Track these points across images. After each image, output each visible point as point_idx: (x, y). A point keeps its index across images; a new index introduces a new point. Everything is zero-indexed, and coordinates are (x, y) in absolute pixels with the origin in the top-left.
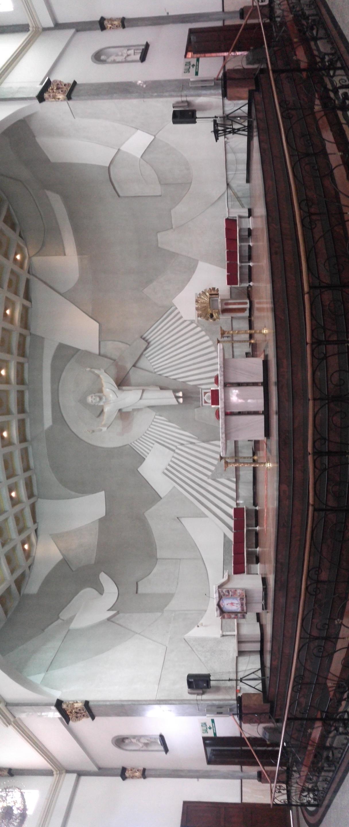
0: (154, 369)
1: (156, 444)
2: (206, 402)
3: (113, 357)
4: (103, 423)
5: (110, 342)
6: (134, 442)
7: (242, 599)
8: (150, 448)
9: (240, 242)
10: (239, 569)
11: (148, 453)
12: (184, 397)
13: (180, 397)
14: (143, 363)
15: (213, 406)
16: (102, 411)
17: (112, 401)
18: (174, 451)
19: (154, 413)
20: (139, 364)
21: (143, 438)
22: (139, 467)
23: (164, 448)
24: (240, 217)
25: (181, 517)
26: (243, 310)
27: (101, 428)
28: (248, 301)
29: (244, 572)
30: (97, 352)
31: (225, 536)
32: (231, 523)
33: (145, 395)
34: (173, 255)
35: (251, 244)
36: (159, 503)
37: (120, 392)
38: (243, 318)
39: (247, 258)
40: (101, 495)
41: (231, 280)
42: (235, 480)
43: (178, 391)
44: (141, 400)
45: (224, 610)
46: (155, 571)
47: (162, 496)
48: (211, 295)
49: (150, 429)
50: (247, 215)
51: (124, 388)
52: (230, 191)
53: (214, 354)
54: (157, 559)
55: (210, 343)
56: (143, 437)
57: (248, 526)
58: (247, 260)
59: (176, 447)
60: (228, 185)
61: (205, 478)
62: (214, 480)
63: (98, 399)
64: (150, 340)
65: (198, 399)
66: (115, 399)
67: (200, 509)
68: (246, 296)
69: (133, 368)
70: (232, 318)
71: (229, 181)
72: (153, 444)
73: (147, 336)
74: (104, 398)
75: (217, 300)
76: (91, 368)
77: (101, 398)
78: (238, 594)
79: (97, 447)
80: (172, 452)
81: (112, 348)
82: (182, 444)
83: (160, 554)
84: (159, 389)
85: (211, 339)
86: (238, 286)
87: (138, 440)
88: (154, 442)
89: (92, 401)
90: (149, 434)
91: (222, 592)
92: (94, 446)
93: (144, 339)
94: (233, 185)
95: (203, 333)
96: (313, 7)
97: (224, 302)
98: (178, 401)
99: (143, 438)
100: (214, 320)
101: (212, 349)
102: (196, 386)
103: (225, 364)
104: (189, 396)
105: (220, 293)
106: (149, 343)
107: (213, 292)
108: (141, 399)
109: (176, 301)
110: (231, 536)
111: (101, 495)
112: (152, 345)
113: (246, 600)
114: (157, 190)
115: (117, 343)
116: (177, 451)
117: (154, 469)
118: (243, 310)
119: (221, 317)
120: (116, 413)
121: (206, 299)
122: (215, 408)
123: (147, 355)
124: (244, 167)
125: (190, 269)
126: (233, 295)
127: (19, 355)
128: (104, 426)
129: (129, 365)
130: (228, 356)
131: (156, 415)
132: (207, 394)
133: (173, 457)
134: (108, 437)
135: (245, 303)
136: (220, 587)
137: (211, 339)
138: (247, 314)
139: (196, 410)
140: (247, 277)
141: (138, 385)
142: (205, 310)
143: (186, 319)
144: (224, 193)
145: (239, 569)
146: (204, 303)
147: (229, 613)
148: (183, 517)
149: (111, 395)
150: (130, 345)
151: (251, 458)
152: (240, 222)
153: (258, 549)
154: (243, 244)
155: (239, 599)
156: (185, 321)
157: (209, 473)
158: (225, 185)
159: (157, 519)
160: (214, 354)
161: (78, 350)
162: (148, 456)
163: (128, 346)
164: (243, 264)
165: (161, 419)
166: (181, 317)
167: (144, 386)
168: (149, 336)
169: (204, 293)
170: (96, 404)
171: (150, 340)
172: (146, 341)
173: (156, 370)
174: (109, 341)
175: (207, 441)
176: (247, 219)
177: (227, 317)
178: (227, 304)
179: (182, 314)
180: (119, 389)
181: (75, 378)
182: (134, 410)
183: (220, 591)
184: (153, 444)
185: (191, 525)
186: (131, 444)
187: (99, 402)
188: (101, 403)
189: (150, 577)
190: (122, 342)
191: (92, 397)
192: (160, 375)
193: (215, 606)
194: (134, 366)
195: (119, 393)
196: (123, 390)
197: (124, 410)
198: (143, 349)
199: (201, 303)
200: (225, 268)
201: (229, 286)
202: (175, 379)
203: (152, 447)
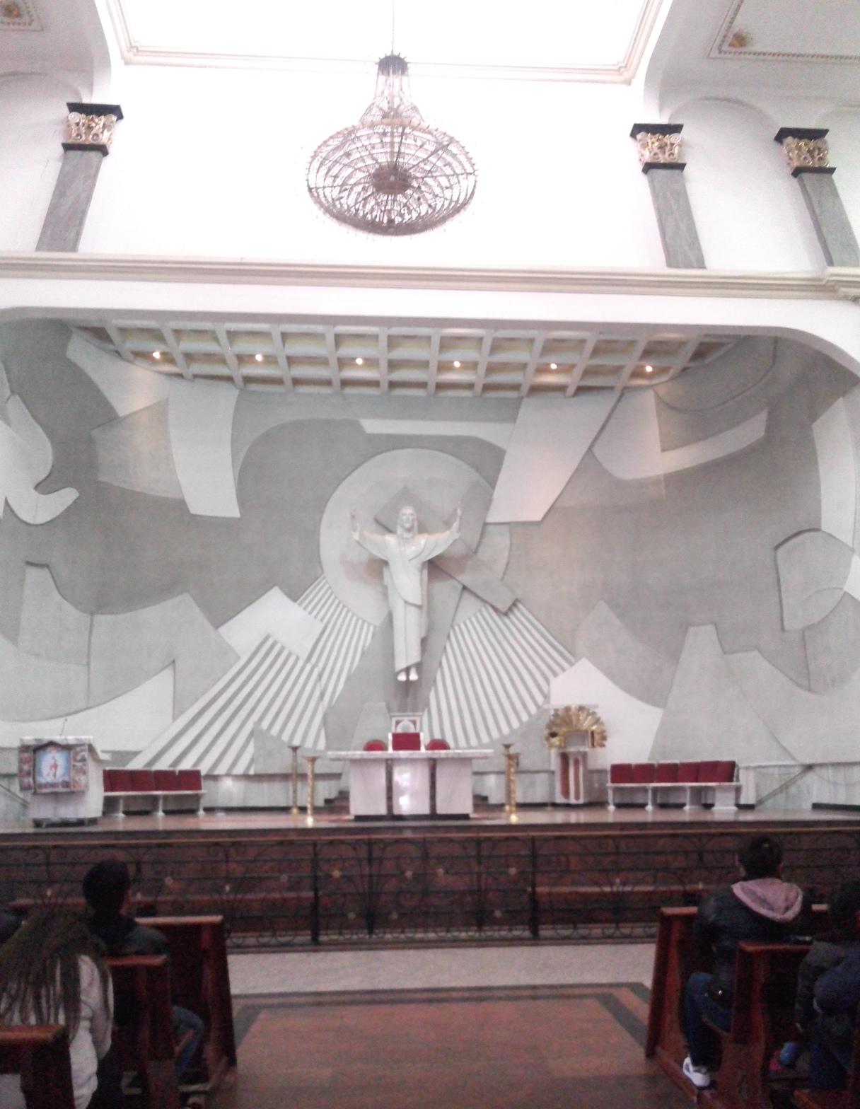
1: (321, 626)
2: (398, 723)
3: (481, 549)
4: (366, 533)
5: (508, 542)
6: (327, 582)
7: (66, 784)
8: (315, 613)
9: (692, 788)
10: (113, 779)
12: (408, 682)
13: (408, 673)
14: (469, 603)
15: (390, 737)
16: (390, 531)
17: (402, 549)
19: (378, 622)
20: (466, 595)
21: (342, 609)
24: (738, 790)
25: (175, 669)
26: (566, 792)
27: (358, 530)
28: (581, 801)
29: (106, 790)
30: (490, 519)
31: (136, 754)
32: (163, 765)
33: (413, 612)
34: (674, 655)
35: (687, 808)
36: (207, 624)
37: (419, 565)
38: (552, 792)
39: (665, 801)
40: (231, 510)
41: (621, 772)
42: (252, 772)
43: (419, 672)
44: (403, 603)
45: (41, 752)
46: (68, 607)
47: (222, 629)
48: (593, 733)
50: (743, 801)
51: (426, 572)
52: (797, 771)
53: (474, 741)
54: (92, 614)
55: (506, 730)
56: (337, 601)
57: (166, 797)
58: (659, 801)
60: (809, 767)
61: (256, 716)
62: (252, 734)
63: (407, 525)
64: (511, 616)
65: (403, 709)
66: (407, 553)
67: (192, 704)
68: (593, 799)
69: (461, 587)
70: (553, 773)
71: (817, 770)
72: (322, 620)
73: (519, 610)
74: (411, 535)
75: (584, 744)
76: (461, 518)
77: (409, 530)
78: (77, 778)
79: (322, 512)
80: (304, 656)
81: (498, 545)
82: (320, 676)
83: (103, 620)
85: (512, 731)
86: (609, 784)
88: (326, 620)
89: (405, 514)
91: (82, 751)
92: (325, 506)
93: (514, 604)
94: (811, 777)
95: (525, 718)
97: (580, 759)
98: (401, 671)
100: (547, 739)
101: (485, 739)
102: (427, 704)
103: (464, 761)
104: (409, 694)
105: (599, 750)
106: (506, 614)
107: (597, 737)
108: (406, 602)
109: (584, 665)
110: (136, 765)
111: (231, 510)
112: (502, 620)
113: (62, 793)
114: (794, 623)
115: (506, 554)
116: (309, 667)
117: (274, 618)
118: (566, 792)
119: (554, 753)
120: (380, 556)
121: (586, 723)
122: (387, 738)
123: (483, 610)
124: (841, 800)
125: (650, 692)
126: (595, 777)
127: (495, 340)
128: (362, 535)
129: (465, 578)
130: (477, 766)
131: (375, 627)
132: (412, 726)
134: (339, 535)
135: (577, 797)
136: (91, 749)
137: (512, 731)
138: (560, 799)
139: (383, 704)
140: (627, 800)
141: (429, 596)
142: (565, 721)
144: (794, 759)
145: (113, 779)
146: (578, 719)
147: (35, 760)
148: (175, 673)
149: (414, 548)
150: (502, 580)
151: (295, 802)
152: (726, 790)
153: (121, 815)
154: (688, 793)
155: (67, 779)
157: (265, 725)
158: (808, 761)
159: (173, 617)
160: (474, 741)
161: (493, 488)
162: (301, 609)
163: (500, 576)
164: (650, 794)
165: (366, 638)
166: (555, 674)
167: (428, 608)
168: (520, 615)
169: (597, 721)
170: (398, 521)
171: (511, 616)
172: (510, 609)
173: (456, 628)
174: (511, 540)
175: (325, 721)
176: (733, 802)
177: (555, 764)
178: (577, 762)
179: (562, 676)
180: (424, 563)
181: (445, 480)
182: (385, 589)
183: (83, 748)
184: (322, 620)
185: (159, 688)
186: (324, 578)
187: (403, 527)
188: (399, 531)
189: (56, 596)
190: (508, 564)
191: (412, 515)
192: (449, 636)
193: (47, 737)
194: (465, 588)
195: (417, 563)
196: (421, 572)
197: (385, 571)
198: (494, 604)
199: (578, 716)
200: (649, 759)
201: (609, 768)
202: (440, 664)
203: (316, 617)
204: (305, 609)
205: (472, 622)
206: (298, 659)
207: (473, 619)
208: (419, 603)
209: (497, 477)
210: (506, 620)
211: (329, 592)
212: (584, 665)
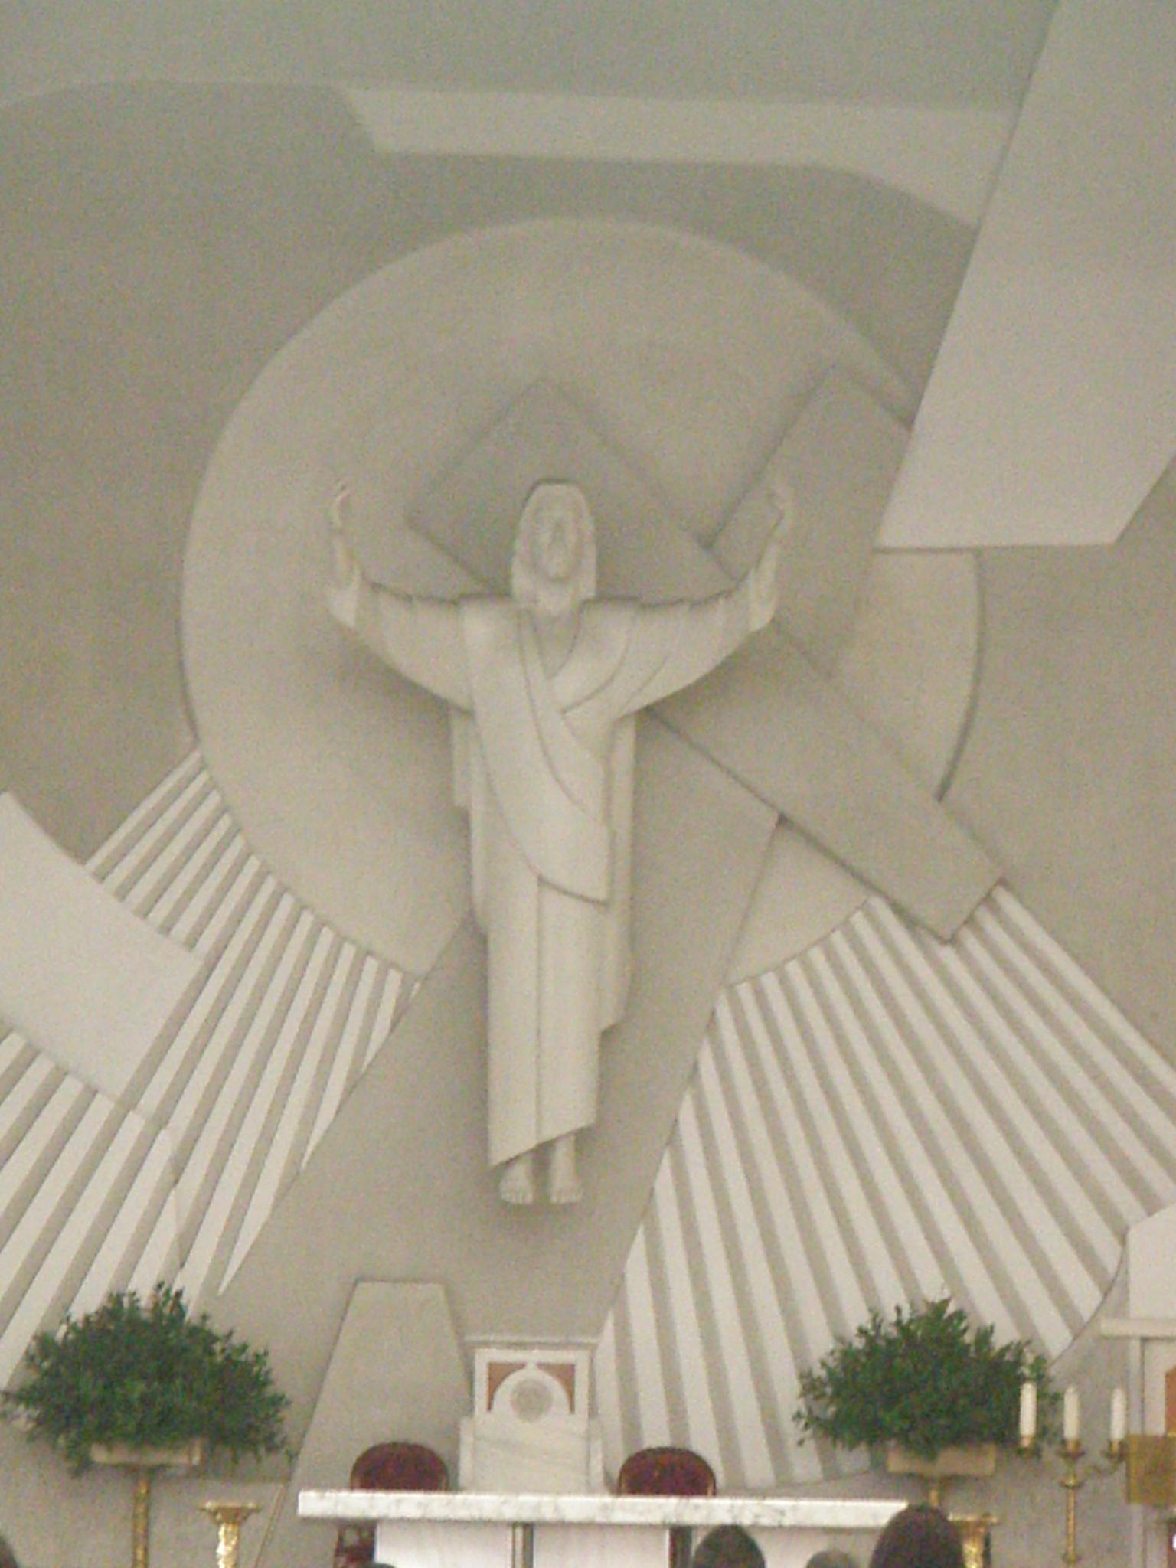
0: (754, 980)
1: (191, 965)
11: (101, 876)
18: (128, 1103)
21: (204, 795)
23: (158, 1025)
49: (307, 921)
59: (161, 1120)
72: (191, 943)
80: (117, 1078)
84: (607, 1021)
88: (206, 942)
90: (207, 830)
99: (204, 795)
108: (541, 881)
116: (134, 1126)
123: (860, 923)
133: (91, 1092)
143: (1133, 1237)
156: (1123, 1238)
184: (191, 943)
194: (783, 820)
203: (166, 929)
207: (817, 956)
208: (601, 894)
211: (225, 822)
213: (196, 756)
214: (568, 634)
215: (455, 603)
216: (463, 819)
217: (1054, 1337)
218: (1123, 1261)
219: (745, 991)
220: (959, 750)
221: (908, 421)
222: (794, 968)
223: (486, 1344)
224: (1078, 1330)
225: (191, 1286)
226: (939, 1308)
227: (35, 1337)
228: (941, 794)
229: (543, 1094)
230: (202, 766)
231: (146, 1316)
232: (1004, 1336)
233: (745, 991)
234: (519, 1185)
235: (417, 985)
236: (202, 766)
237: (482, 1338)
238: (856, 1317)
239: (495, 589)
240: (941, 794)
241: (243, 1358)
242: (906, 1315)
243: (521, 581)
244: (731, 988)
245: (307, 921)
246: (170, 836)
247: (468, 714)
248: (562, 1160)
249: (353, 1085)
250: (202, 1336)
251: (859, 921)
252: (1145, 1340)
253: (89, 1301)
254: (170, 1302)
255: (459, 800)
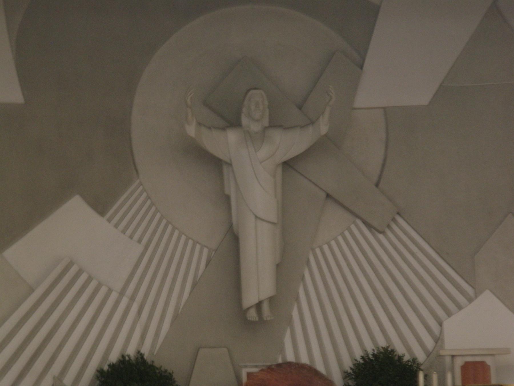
1: (140, 248)
8: (129, 232)
11: (124, 232)
18: (122, 293)
21: (141, 194)
22: (85, 198)
59: (132, 299)
72: (139, 241)
80: (118, 286)
87: (149, 202)
96: (103, 379)
108: (256, 217)
109: (487, 298)
116: (125, 301)
133: (110, 291)
143: (445, 324)
156: (441, 324)
184: (139, 241)
194: (328, 196)
203: (131, 237)
204: (116, 226)
205: (330, 247)
206: (110, 291)
207: (340, 239)
208: (275, 221)
209: (368, 43)
210: (381, 237)
211: (149, 202)
212: (487, 298)
213: (138, 181)
214: (259, 138)
215: (224, 129)
216: (228, 198)
217: (421, 357)
218: (441, 332)
219: (318, 251)
220: (382, 171)
221: (361, 67)
222: (333, 243)
223: (246, 367)
224: (428, 354)
225: (145, 350)
226: (386, 349)
227: (97, 371)
228: (377, 185)
229: (259, 285)
230: (141, 184)
231: (134, 362)
232: (407, 358)
233: (318, 251)
234: (252, 315)
235: (213, 253)
236: (141, 184)
237: (244, 364)
238: (358, 354)
239: (234, 123)
240: (377, 185)
241: (166, 374)
242: (376, 352)
243: (245, 121)
244: (313, 250)
245: (176, 233)
246: (131, 207)
247: (230, 164)
248: (266, 307)
249: (195, 285)
250: (152, 367)
251: (353, 227)
252: (453, 356)
253: (114, 357)
254: (140, 355)
255: (227, 192)
